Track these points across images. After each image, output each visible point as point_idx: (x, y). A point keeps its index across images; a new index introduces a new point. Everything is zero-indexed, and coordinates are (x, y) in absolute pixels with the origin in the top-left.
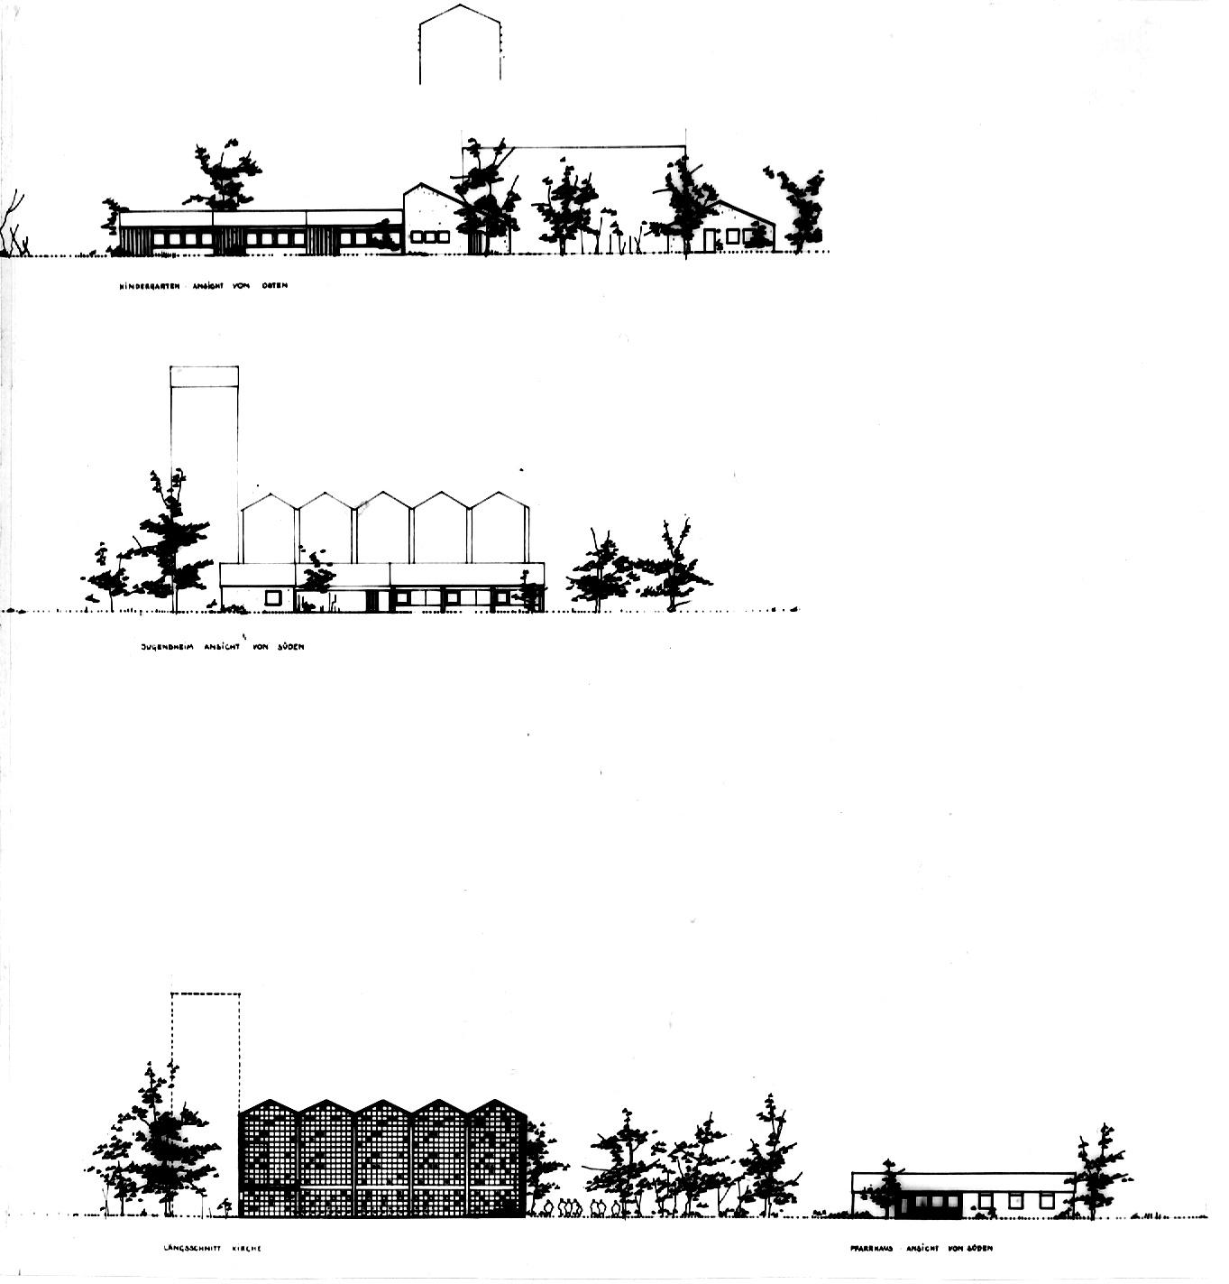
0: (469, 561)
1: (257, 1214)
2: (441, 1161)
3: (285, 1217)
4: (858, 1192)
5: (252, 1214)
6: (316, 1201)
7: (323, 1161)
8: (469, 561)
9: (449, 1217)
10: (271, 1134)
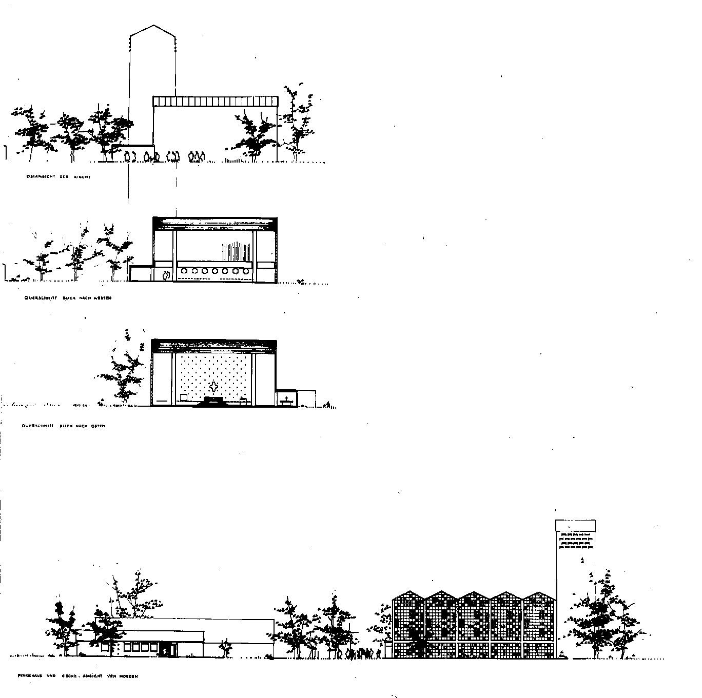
0: (152, 280)
1: (411, 656)
2: (431, 611)
3: (438, 658)
4: (111, 654)
5: (408, 656)
6: (482, 647)
7: (508, 621)
8: (152, 280)
9: (506, 659)
10: (463, 614)
